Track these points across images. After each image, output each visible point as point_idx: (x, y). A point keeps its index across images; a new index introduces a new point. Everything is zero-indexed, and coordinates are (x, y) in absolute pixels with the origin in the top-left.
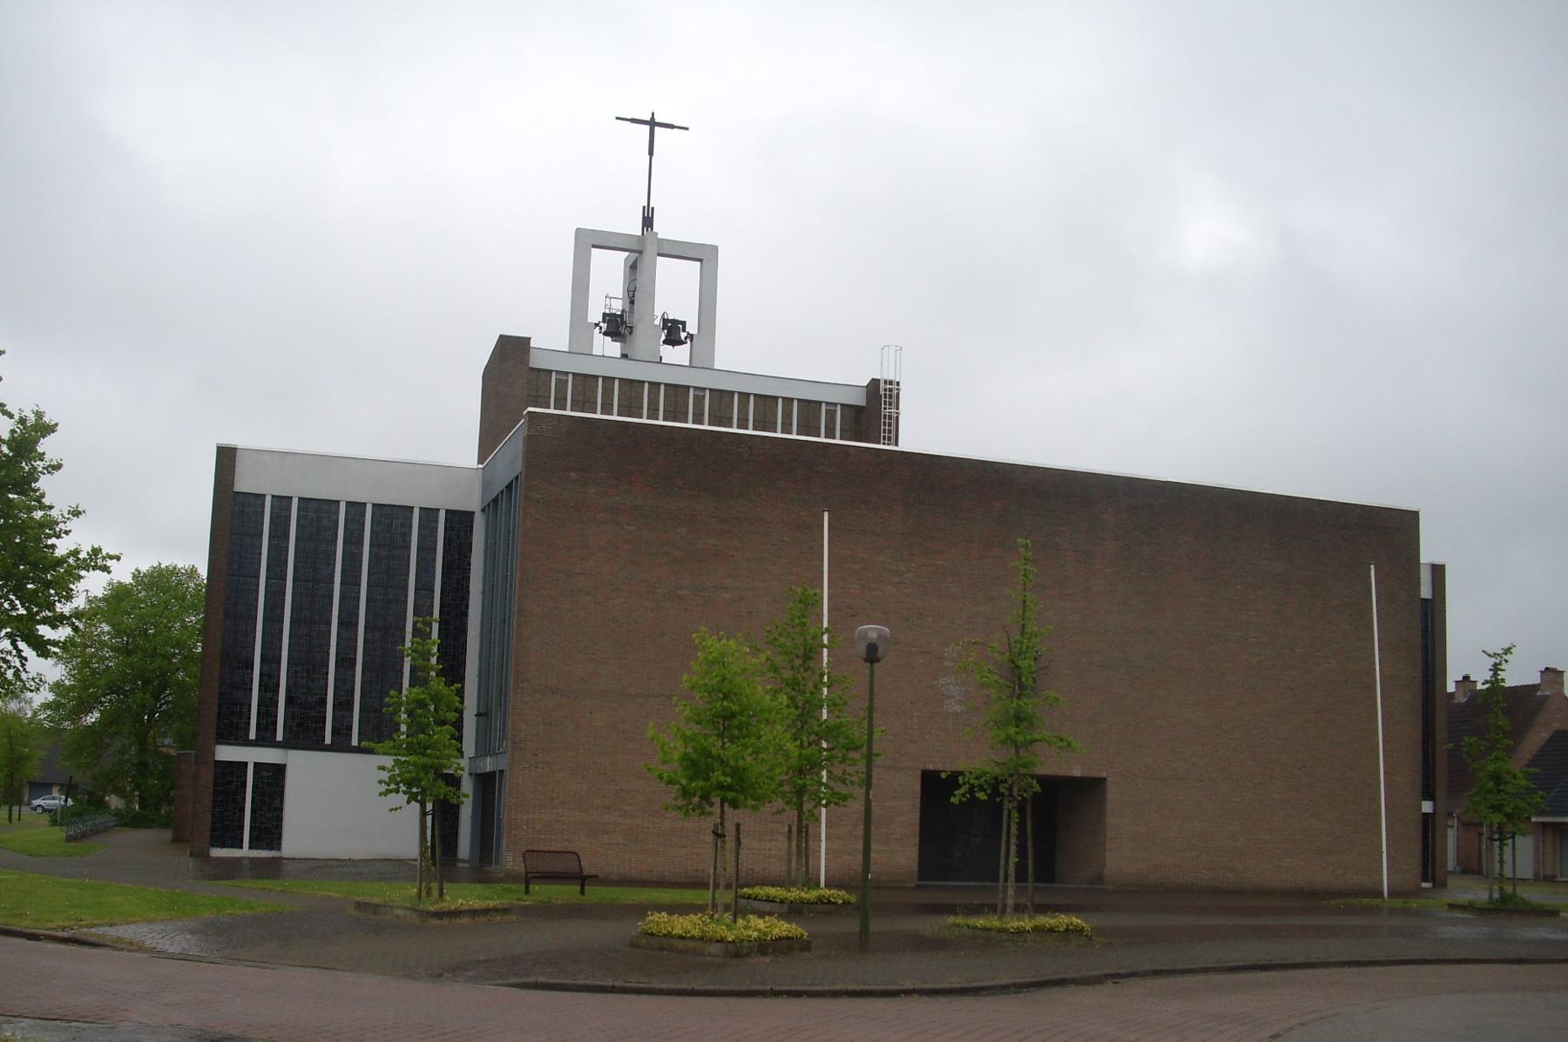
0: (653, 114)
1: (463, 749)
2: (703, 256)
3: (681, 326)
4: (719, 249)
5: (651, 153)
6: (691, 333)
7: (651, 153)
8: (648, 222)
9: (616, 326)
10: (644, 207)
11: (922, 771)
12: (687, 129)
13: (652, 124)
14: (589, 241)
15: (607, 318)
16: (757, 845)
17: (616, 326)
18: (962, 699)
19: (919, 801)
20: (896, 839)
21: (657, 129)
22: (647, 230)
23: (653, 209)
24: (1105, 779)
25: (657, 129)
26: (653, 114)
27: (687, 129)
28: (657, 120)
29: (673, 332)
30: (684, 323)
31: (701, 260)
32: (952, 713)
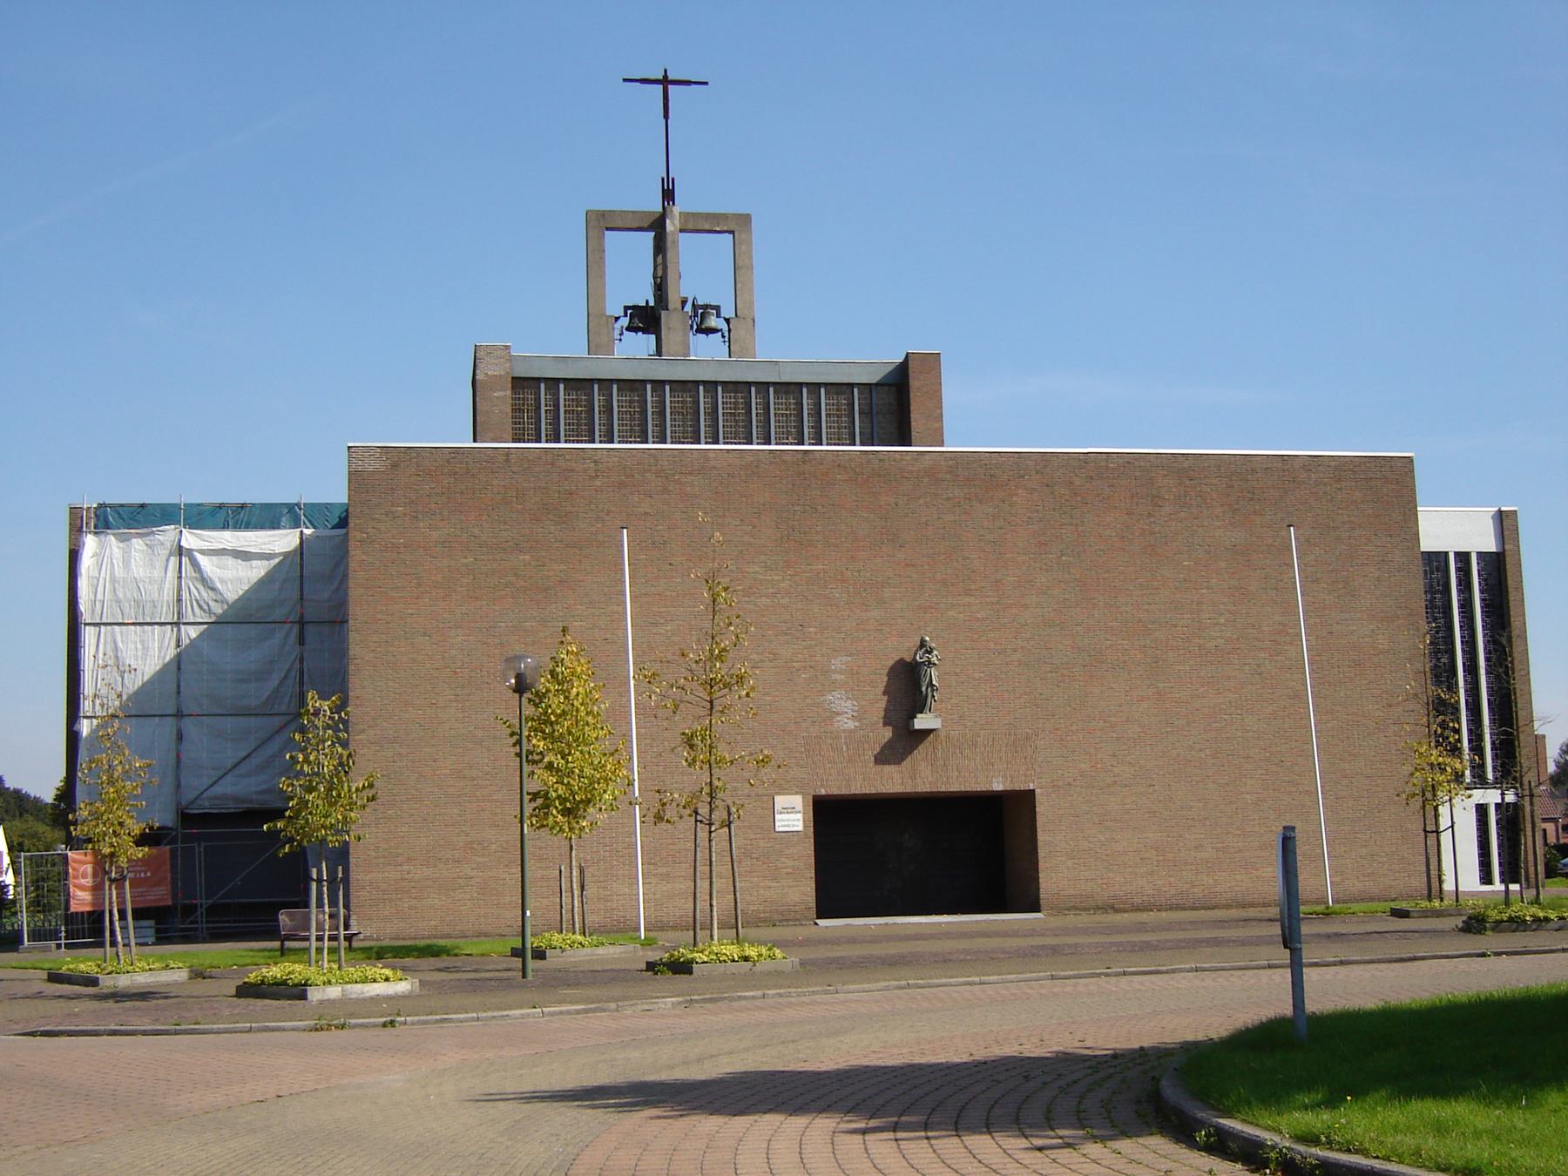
0: (666, 71)
1: (535, 791)
2: (734, 226)
3: (714, 312)
4: (753, 217)
5: (666, 116)
6: (727, 317)
7: (666, 116)
8: (668, 195)
9: (646, 319)
10: (663, 179)
11: (814, 796)
12: (625, 80)
13: (665, 82)
14: (602, 223)
15: (629, 312)
16: (627, 890)
17: (646, 319)
18: (855, 714)
19: (812, 829)
20: (788, 874)
21: (670, 87)
22: (668, 204)
23: (673, 180)
24: (1033, 791)
25: (670, 87)
26: (666, 71)
27: (625, 80)
28: (671, 77)
29: (701, 318)
30: (717, 308)
31: (732, 232)
32: (844, 731)
